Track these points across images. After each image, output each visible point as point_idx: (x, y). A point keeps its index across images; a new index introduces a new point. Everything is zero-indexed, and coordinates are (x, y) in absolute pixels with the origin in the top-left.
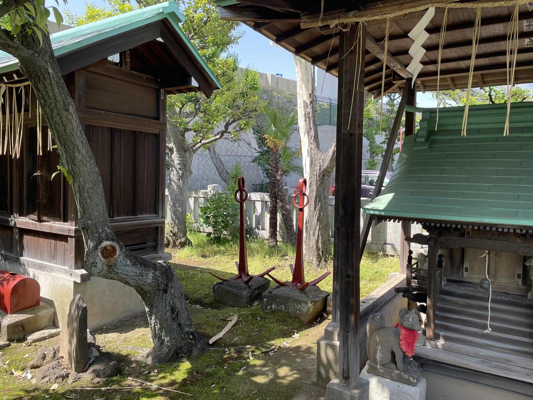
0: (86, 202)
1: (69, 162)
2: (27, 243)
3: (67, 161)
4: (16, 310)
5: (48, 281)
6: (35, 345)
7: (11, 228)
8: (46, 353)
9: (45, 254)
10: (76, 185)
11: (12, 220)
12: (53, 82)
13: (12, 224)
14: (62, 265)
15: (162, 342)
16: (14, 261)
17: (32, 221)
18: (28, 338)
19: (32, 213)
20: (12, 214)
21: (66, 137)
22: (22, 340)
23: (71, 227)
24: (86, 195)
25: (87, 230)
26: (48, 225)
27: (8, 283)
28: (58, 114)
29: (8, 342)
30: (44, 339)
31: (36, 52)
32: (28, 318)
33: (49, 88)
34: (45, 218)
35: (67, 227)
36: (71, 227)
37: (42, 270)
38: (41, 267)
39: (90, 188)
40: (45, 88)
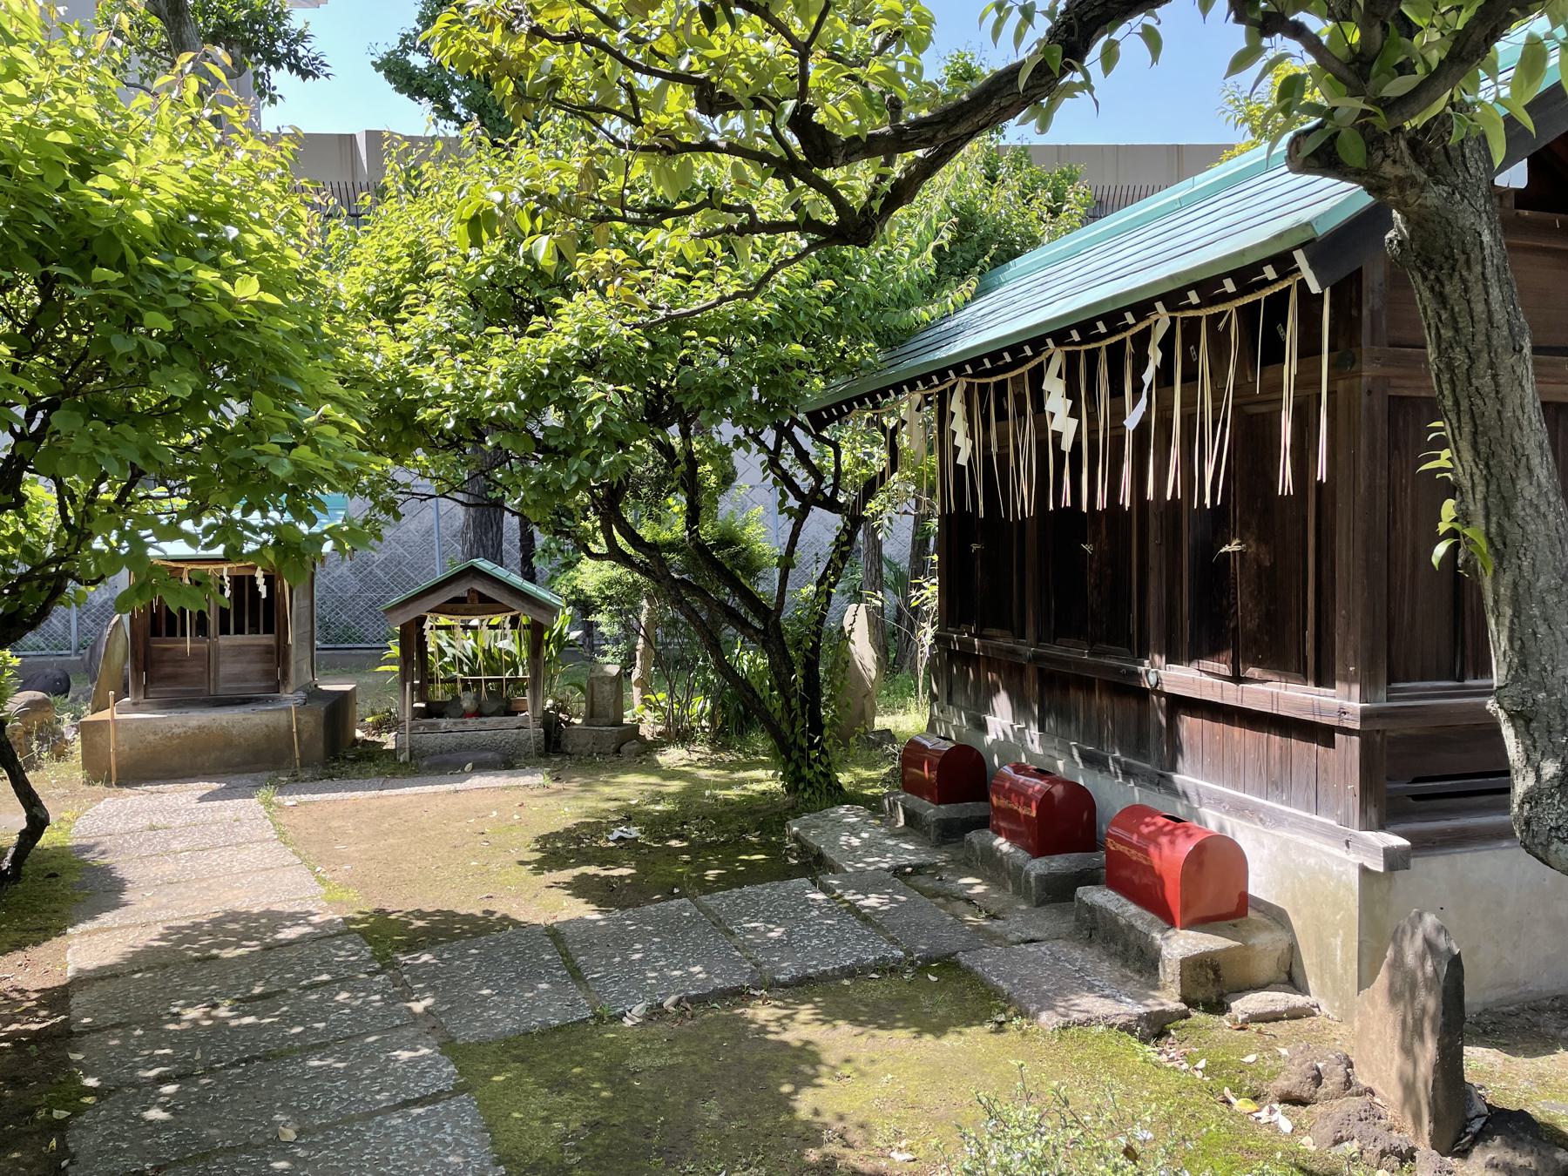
0: (1535, 634)
1: (1493, 511)
2: (1191, 737)
3: (1487, 508)
4: (1202, 923)
5: (1266, 852)
6: (1259, 1032)
7: (1143, 695)
8: (1320, 1065)
9: (1249, 772)
10: (1507, 579)
11: (1147, 672)
12: (1489, 271)
13: (1149, 682)
14: (1308, 810)
15: (948, 1017)
16: (1151, 782)
17: (1210, 679)
18: (1233, 1005)
19: (1213, 652)
20: (1143, 654)
21: (1498, 434)
22: (1218, 1007)
23: (1346, 703)
24: (1536, 611)
25: (1528, 721)
26: (1263, 692)
27: (1172, 842)
28: (1492, 365)
29: (1183, 1007)
30: (1275, 1017)
31: (1455, 188)
32: (1228, 950)
33: (1477, 289)
34: (1253, 672)
35: (1341, 702)
36: (1346, 703)
37: (1242, 817)
38: (1239, 809)
39: (1549, 591)
40: (1466, 290)
